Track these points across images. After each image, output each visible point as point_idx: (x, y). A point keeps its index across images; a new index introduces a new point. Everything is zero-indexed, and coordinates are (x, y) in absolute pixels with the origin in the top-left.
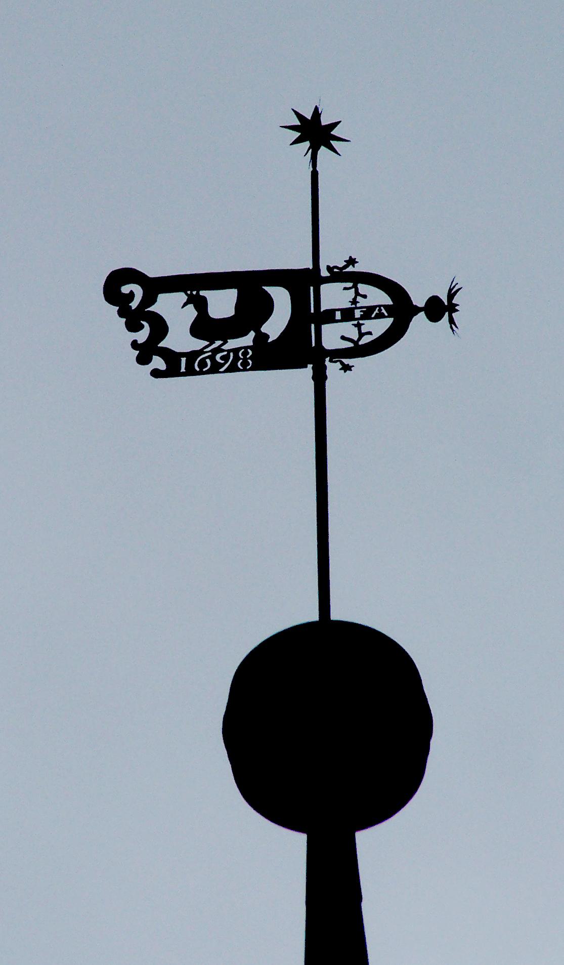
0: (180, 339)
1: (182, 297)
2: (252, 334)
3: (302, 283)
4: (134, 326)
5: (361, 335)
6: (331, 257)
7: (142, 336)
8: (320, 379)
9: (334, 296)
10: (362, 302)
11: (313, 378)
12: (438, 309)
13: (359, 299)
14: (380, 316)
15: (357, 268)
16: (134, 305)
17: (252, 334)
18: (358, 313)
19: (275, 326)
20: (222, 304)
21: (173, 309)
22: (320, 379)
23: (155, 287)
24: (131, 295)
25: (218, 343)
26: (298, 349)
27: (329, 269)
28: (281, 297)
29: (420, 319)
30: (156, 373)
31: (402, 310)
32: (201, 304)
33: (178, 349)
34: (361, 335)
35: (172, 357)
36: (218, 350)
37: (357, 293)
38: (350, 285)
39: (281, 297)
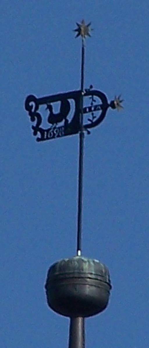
0: (45, 125)
1: (45, 106)
2: (64, 121)
3: (77, 96)
4: (33, 120)
5: (94, 118)
6: (86, 87)
7: (35, 123)
8: (82, 136)
9: (87, 102)
10: (95, 104)
11: (46, 287)
12: (113, 105)
13: (94, 102)
14: (99, 109)
15: (93, 89)
16: (33, 110)
17: (64, 121)
18: (93, 109)
19: (70, 117)
20: (57, 107)
21: (43, 111)
22: (82, 136)
23: (39, 102)
24: (32, 106)
25: (55, 124)
26: (74, 127)
27: (86, 90)
28: (72, 102)
29: (110, 108)
30: (38, 140)
31: (104, 107)
32: (50, 108)
33: (44, 129)
34: (94, 118)
35: (42, 131)
36: (55, 128)
37: (93, 100)
38: (90, 96)
39: (72, 102)
